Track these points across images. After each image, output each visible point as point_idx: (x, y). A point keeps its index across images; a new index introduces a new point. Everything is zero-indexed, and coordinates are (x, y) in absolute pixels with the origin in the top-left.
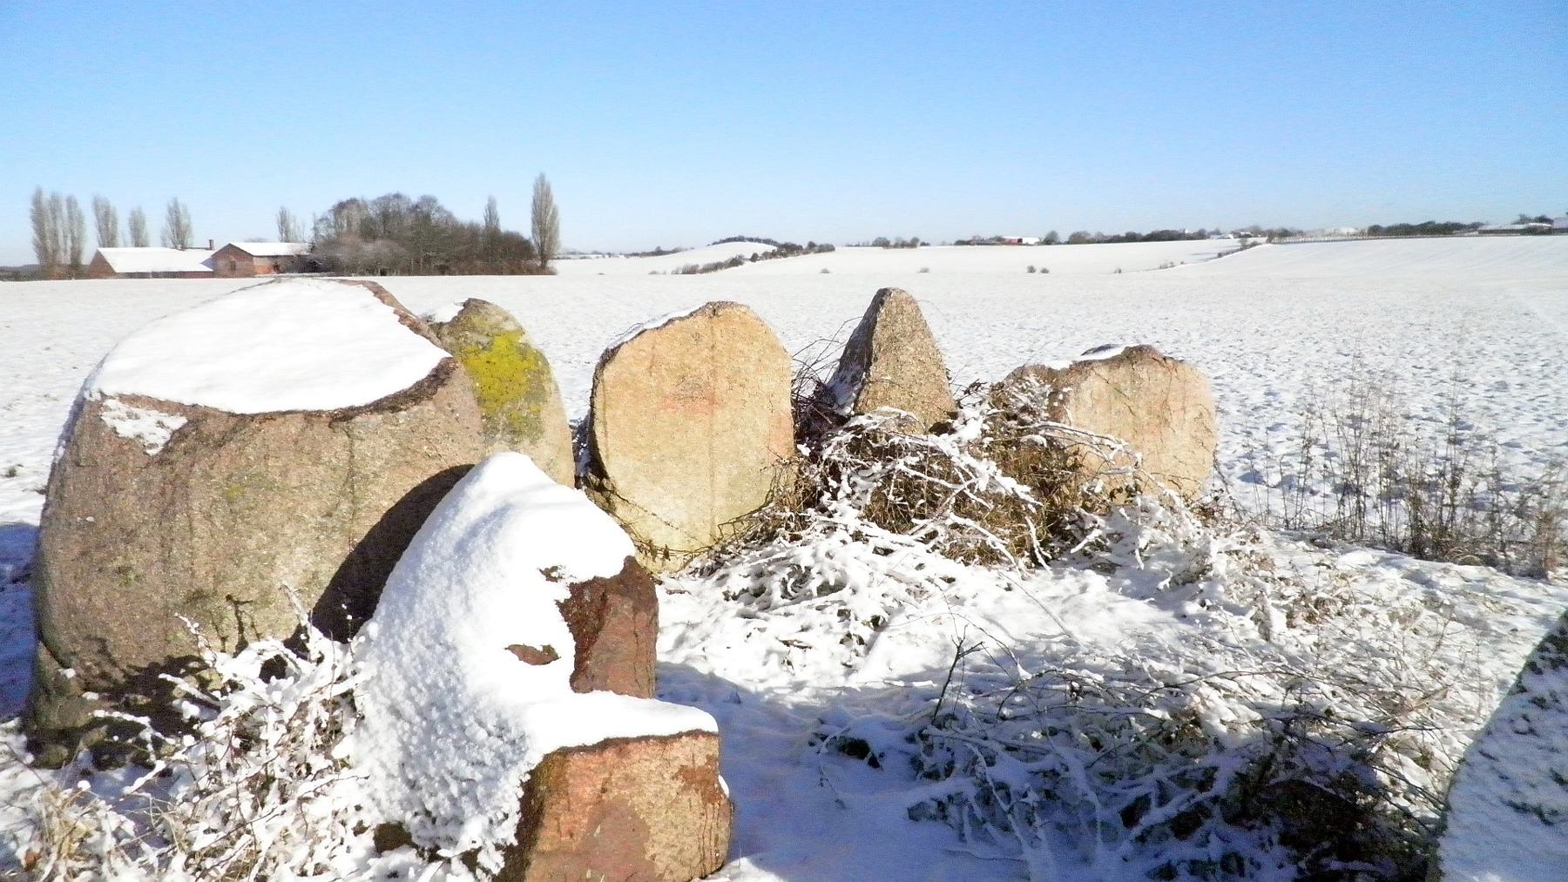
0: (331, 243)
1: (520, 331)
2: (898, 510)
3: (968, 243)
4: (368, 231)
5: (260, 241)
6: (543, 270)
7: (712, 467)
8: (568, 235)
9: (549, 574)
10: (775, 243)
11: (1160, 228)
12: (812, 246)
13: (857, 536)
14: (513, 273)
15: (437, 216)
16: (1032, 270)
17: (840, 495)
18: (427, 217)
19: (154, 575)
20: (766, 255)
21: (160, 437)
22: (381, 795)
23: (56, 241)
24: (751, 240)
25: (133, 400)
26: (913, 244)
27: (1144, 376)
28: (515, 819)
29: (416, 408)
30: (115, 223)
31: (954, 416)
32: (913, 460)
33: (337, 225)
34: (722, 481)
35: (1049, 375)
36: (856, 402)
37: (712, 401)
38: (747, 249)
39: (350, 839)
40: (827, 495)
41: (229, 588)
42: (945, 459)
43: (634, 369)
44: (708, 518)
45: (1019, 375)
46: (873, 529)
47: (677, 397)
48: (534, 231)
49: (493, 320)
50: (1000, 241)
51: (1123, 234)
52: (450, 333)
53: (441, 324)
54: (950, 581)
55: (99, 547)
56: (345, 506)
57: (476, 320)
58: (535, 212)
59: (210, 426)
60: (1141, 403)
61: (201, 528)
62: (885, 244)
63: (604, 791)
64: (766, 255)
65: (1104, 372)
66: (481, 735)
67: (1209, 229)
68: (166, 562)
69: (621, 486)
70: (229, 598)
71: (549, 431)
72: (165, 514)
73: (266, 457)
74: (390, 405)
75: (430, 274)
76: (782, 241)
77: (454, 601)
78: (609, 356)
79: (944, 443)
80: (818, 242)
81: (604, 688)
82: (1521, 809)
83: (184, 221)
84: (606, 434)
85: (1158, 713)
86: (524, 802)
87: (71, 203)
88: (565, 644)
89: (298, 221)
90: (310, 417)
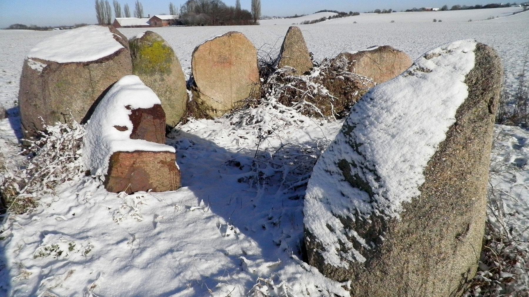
0: (185, 15)
1: (163, 41)
2: (289, 98)
3: (411, 11)
4: (198, 11)
5: (164, 14)
6: (255, 23)
7: (231, 84)
8: (264, 11)
9: (128, 107)
10: (337, 12)
11: (490, 2)
12: (351, 13)
13: (275, 107)
14: (245, 24)
15: (220, 5)
16: (435, 21)
17: (271, 94)
18: (217, 5)
19: (42, 107)
20: (334, 17)
21: (40, 69)
22: (86, 163)
23: (103, 16)
24: (329, 11)
25: (34, 59)
26: (389, 12)
27: (385, 56)
28: (107, 168)
29: (107, 62)
30: (120, 9)
31: (312, 69)
32: (294, 83)
33: (188, 9)
34: (234, 89)
35: (350, 57)
36: (278, 64)
37: (230, 64)
38: (327, 15)
39: (79, 174)
40: (268, 94)
41: (61, 110)
42: (304, 83)
43: (204, 53)
44: (230, 100)
45: (340, 56)
46: (280, 105)
47: (218, 62)
48: (252, 9)
49: (153, 38)
50: (423, 10)
51: (474, 6)
52: (140, 42)
53: (138, 39)
54: (302, 122)
55: (30, 99)
56: (90, 90)
57: (148, 37)
58: (252, 3)
59: (53, 67)
60: (384, 66)
61: (52, 94)
62: (378, 12)
63: (134, 164)
64: (334, 17)
65: (369, 55)
66: (103, 147)
67: (511, 3)
68: (45, 103)
69: (202, 89)
70: (61, 113)
71: (174, 72)
72: (43, 90)
73: (67, 75)
74: (100, 61)
75: (217, 25)
76: (340, 11)
77: (104, 113)
78: (196, 49)
79: (305, 78)
80: (353, 11)
81: (143, 138)
82: (327, 171)
83: (141, 8)
84: (196, 73)
85: (313, 156)
86: (109, 163)
87: (107, 3)
88: (130, 125)
89: (176, 7)
90: (78, 64)
